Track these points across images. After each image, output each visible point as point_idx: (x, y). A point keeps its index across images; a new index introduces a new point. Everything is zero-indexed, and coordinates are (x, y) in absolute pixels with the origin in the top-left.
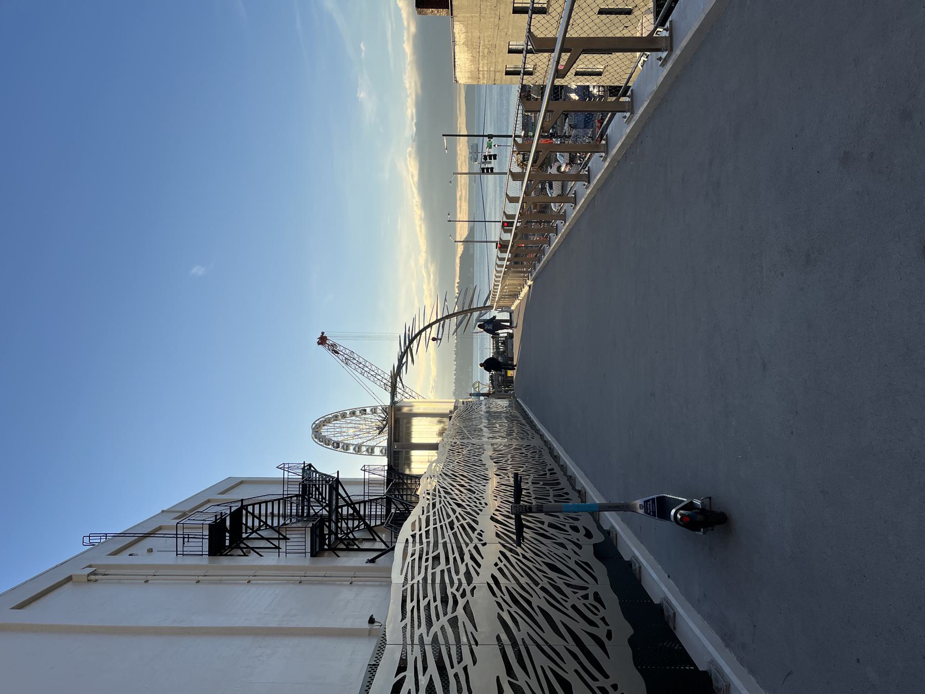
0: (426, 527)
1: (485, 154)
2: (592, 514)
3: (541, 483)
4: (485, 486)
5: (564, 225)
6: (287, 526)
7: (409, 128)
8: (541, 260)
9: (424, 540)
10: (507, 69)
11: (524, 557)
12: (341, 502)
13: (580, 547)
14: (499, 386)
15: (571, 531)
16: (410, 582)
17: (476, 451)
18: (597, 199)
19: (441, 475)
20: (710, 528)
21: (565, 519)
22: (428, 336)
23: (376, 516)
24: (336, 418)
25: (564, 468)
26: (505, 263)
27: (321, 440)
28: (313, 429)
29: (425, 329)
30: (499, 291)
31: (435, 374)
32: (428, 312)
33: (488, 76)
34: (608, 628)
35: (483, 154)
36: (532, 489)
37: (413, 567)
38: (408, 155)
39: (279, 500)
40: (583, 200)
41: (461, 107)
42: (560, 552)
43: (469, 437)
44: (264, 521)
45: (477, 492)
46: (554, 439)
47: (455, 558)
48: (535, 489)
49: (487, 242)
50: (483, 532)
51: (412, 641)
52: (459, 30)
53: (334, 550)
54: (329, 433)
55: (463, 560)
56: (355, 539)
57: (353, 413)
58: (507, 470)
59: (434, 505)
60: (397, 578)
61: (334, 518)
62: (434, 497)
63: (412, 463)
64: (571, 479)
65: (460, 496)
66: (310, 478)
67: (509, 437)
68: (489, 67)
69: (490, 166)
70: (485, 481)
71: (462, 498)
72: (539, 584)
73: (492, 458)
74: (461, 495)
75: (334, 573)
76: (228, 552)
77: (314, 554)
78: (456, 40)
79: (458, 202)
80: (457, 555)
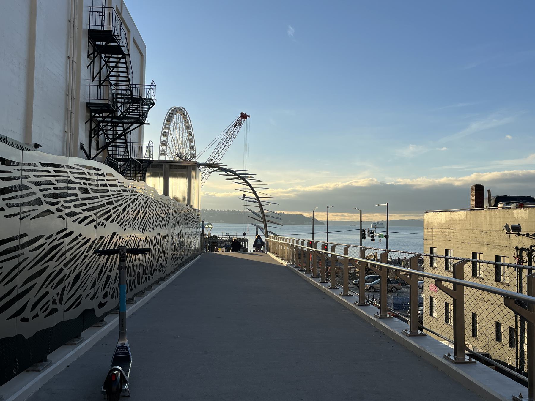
0: (107, 186)
1: (375, 233)
2: (118, 308)
3: (140, 271)
4: (138, 229)
5: (327, 288)
6: (109, 86)
7: (389, 180)
8: (302, 272)
9: (100, 183)
10: (434, 248)
11: (86, 257)
12: (126, 126)
13: (92, 299)
14: (209, 242)
15: (104, 292)
16: (69, 170)
17: (164, 224)
18: (347, 311)
19: (147, 197)
20: (106, 396)
21: (113, 288)
22: (246, 190)
23: (115, 151)
25: (150, 288)
26: (300, 246)
27: (171, 115)
28: (179, 108)
29: (252, 188)
30: (279, 241)
31: (217, 196)
33: (429, 235)
34: (30, 320)
35: (375, 232)
36: (135, 264)
37: (80, 173)
38: (371, 179)
39: (129, 81)
40: (346, 301)
41: (406, 217)
42: (89, 284)
43: (174, 219)
44: (114, 70)
45: (134, 223)
46: (171, 281)
47: (86, 205)
48: (135, 265)
49: (313, 234)
50: (105, 226)
51: (25, 170)
52: (461, 215)
53: (91, 120)
55: (84, 210)
56: (99, 135)
57: (190, 134)
58: (149, 246)
59: (125, 191)
60: (73, 161)
61: (115, 120)
62: (130, 192)
63: (154, 178)
64: (141, 294)
65: (131, 210)
66: (145, 104)
67: (173, 248)
68: (435, 236)
69: (366, 236)
70: (142, 229)
71: (130, 212)
72: (65, 267)
73: (158, 235)
74: (132, 211)
75: (73, 120)
76: (90, 43)
77: (88, 105)
78: (454, 213)
79: (340, 214)
80: (88, 206)
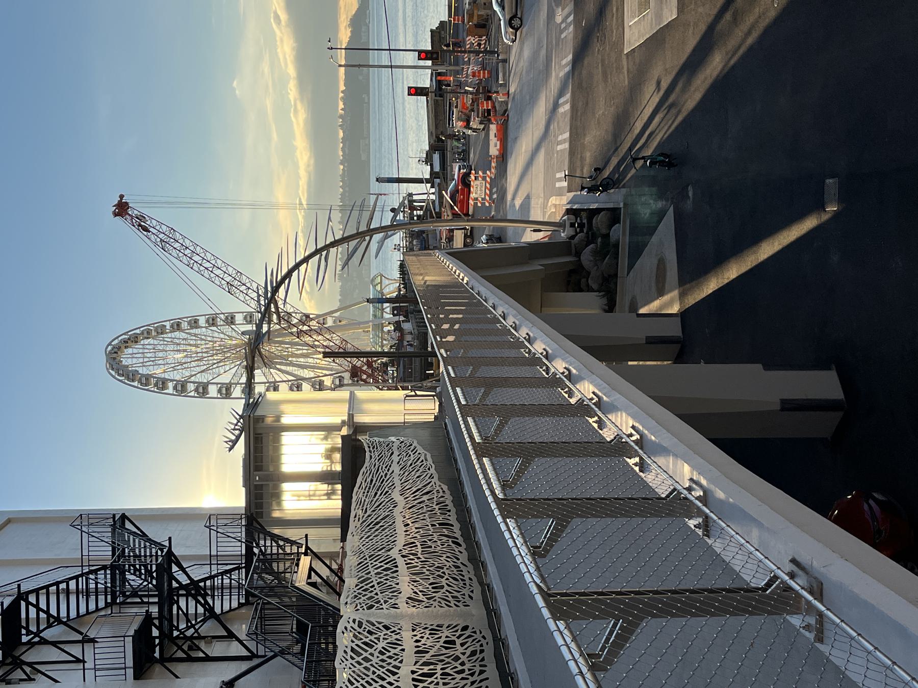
24: (148, 334)
27: (121, 372)
29: (297, 266)
32: (301, 242)
49: (391, 67)
54: (135, 361)
57: (177, 327)
